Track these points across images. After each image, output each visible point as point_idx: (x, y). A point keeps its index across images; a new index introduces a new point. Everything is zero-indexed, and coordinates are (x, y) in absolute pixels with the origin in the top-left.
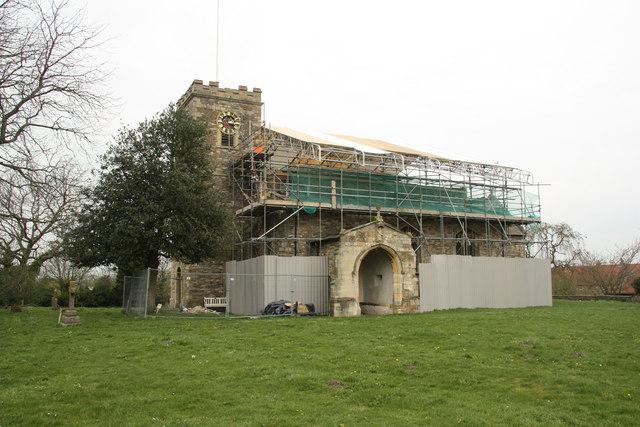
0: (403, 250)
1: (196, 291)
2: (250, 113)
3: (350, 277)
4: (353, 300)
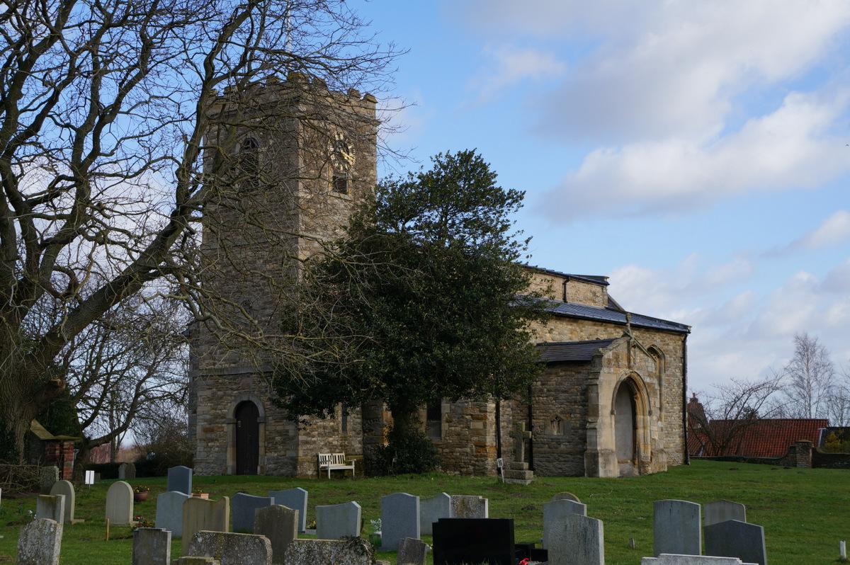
4: (606, 407)
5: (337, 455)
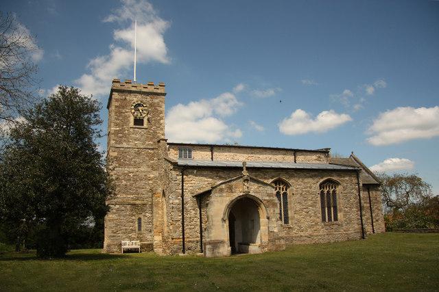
0: (267, 198)
1: (114, 236)
2: (156, 101)
3: (220, 223)
4: (222, 242)
5: (134, 242)
